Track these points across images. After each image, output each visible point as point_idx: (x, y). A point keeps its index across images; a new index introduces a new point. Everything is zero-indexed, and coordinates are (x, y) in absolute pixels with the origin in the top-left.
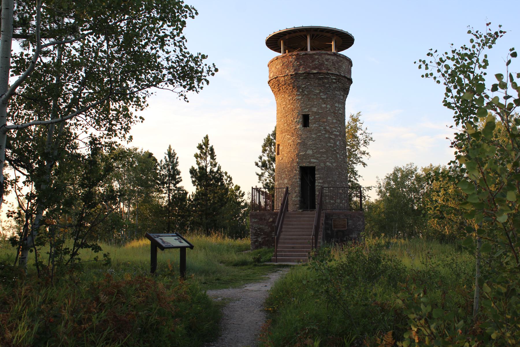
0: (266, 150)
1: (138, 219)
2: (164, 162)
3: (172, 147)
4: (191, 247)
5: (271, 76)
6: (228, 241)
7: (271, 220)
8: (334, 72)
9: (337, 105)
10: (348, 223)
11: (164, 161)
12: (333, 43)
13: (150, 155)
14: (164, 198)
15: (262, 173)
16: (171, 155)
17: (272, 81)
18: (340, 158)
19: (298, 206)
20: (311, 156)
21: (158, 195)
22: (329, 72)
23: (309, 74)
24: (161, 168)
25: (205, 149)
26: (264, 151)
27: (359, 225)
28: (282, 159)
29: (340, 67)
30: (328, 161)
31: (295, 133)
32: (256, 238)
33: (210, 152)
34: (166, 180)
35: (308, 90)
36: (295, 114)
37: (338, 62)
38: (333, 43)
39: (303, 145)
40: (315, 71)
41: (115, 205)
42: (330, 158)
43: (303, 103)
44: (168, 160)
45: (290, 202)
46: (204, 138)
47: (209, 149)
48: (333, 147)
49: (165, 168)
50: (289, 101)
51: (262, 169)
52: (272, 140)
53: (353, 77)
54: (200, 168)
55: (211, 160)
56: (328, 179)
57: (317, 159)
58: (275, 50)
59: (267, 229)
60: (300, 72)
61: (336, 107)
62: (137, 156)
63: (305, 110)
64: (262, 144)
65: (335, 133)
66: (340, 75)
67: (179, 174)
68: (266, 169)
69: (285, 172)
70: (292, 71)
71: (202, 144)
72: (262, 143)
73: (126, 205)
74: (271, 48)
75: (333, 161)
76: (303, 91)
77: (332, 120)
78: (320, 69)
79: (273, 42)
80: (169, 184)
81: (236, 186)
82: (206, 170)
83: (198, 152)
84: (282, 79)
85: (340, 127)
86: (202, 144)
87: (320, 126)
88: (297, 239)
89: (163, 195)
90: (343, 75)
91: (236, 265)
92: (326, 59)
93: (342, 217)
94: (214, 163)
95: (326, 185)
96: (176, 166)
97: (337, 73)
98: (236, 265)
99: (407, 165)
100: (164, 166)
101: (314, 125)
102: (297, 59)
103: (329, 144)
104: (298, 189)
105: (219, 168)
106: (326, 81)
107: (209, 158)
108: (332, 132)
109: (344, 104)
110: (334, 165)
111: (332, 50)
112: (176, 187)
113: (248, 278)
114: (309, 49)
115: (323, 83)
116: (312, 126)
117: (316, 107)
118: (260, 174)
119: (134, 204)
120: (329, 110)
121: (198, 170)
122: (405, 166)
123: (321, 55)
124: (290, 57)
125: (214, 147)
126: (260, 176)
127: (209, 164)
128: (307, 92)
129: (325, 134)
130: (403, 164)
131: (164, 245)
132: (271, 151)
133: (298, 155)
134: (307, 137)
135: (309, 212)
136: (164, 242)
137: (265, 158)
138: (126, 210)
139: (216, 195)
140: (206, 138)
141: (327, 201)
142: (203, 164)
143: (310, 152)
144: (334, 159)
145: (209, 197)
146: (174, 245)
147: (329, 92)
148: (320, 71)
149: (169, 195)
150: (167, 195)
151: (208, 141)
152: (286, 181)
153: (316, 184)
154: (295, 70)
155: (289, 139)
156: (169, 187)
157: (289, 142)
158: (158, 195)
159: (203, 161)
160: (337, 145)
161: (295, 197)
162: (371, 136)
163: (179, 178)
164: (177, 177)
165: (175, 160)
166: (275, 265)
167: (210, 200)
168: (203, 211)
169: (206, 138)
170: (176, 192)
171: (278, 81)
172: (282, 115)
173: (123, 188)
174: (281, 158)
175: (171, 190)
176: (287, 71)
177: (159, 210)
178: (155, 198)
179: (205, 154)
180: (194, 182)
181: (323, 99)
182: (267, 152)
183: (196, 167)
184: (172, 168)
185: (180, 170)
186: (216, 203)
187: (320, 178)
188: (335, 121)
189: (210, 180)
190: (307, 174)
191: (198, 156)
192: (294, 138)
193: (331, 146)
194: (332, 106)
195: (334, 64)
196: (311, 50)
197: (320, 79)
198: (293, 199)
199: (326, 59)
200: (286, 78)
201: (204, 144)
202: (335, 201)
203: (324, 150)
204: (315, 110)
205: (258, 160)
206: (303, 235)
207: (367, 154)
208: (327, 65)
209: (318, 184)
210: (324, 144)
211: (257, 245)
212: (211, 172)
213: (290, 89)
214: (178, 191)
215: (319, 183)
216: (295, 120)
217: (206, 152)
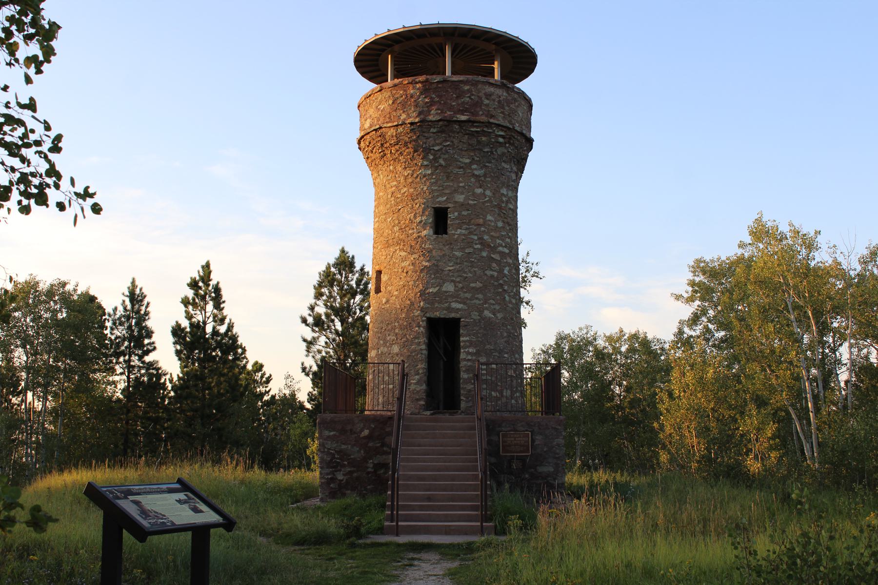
0: (322, 295)
1: (62, 424)
2: (120, 311)
3: (137, 283)
4: (229, 524)
5: (367, 125)
6: (258, 474)
7: (366, 432)
10: (533, 441)
11: (120, 309)
12: (496, 65)
13: (93, 299)
14: (117, 384)
15: (314, 338)
16: (135, 297)
17: (368, 137)
18: (510, 302)
19: (422, 403)
20: (452, 296)
21: (105, 377)
22: (492, 120)
23: (449, 122)
24: (114, 324)
25: (204, 289)
26: (319, 295)
27: (558, 445)
28: (387, 302)
29: (513, 112)
30: (487, 309)
31: (418, 246)
32: (332, 473)
33: (213, 295)
34: (123, 348)
35: (446, 156)
36: (418, 206)
37: (509, 103)
38: (496, 65)
39: (434, 272)
41: (18, 395)
42: (492, 301)
43: (436, 183)
44: (129, 307)
46: (203, 267)
47: (210, 288)
48: (497, 279)
49: (121, 324)
50: (406, 178)
51: (313, 331)
52: (335, 274)
53: (533, 135)
54: (192, 325)
55: (215, 311)
56: (488, 347)
57: (464, 303)
58: (371, 79)
59: (357, 453)
60: (431, 118)
61: (503, 194)
62: (66, 300)
64: (315, 283)
65: (501, 248)
66: (513, 130)
67: (150, 337)
68: (322, 329)
69: (394, 328)
70: (414, 114)
71: (198, 278)
72: (315, 279)
73: (39, 397)
74: (363, 74)
75: (497, 307)
76: (436, 159)
77: (496, 221)
78: (473, 114)
79: (371, 60)
80: (130, 356)
81: (256, 363)
82: (204, 328)
83: (190, 294)
84: (392, 131)
85: (509, 237)
86: (198, 278)
87: (471, 233)
88: (435, 478)
89: (116, 378)
90: (518, 129)
91: (301, 542)
92: (485, 94)
93: (522, 429)
94: (220, 317)
95: (483, 360)
96: (145, 320)
98: (301, 542)
99: (581, 329)
100: (119, 319)
101: (459, 231)
102: (425, 91)
103: (489, 273)
104: (422, 366)
105: (230, 327)
106: (484, 139)
107: (210, 307)
108: (495, 247)
109: (515, 189)
110: (500, 315)
111: (444, 73)
112: (143, 362)
114: (448, 72)
115: (479, 142)
116: (455, 232)
117: (462, 193)
118: (309, 339)
119: (56, 396)
120: (490, 201)
121: (188, 330)
122: (577, 330)
123: (475, 84)
124: (411, 87)
125: (221, 286)
126: (310, 344)
127: (211, 319)
128: (445, 160)
129: (481, 250)
130: (571, 328)
131: (145, 523)
132: (330, 296)
133: (422, 293)
134: (444, 255)
135: (447, 416)
136: (145, 513)
137: (321, 310)
138: (38, 405)
139: (222, 379)
140: (207, 267)
142: (199, 318)
143: (449, 287)
144: (500, 304)
145: (210, 383)
146: (179, 522)
148: (473, 118)
149: (128, 377)
150: (124, 377)
151: (210, 272)
152: (396, 349)
153: (462, 356)
154: (420, 114)
155: (404, 259)
156: (129, 360)
157: (403, 264)
158: (105, 377)
159: (198, 312)
160: (505, 275)
161: (417, 384)
162: (535, 268)
163: (149, 344)
164: (146, 341)
165: (143, 308)
166: (399, 545)
167: (210, 388)
168: (196, 410)
169: (207, 267)
170: (143, 371)
171: (382, 136)
172: (386, 210)
173: (34, 361)
174: (384, 300)
175: (134, 367)
176: (404, 116)
177: (106, 408)
178: (99, 383)
179: (203, 298)
180: (178, 353)
182: (324, 298)
183: (185, 324)
184: (137, 324)
185: (153, 329)
186: (222, 395)
187: (471, 344)
189: (212, 351)
190: (442, 334)
191: (189, 303)
192: (416, 256)
193: (492, 276)
194: (495, 192)
195: (501, 105)
197: (472, 134)
198: (412, 387)
199: (485, 94)
200: (400, 129)
201: (202, 279)
202: (501, 393)
203: (478, 285)
204: (460, 198)
205: (306, 313)
206: (447, 469)
207: (527, 303)
208: (487, 105)
209: (465, 355)
210: (479, 272)
211: (333, 488)
212: (215, 332)
213: (409, 154)
214: (148, 369)
215: (468, 353)
216: (418, 219)
217: (206, 294)
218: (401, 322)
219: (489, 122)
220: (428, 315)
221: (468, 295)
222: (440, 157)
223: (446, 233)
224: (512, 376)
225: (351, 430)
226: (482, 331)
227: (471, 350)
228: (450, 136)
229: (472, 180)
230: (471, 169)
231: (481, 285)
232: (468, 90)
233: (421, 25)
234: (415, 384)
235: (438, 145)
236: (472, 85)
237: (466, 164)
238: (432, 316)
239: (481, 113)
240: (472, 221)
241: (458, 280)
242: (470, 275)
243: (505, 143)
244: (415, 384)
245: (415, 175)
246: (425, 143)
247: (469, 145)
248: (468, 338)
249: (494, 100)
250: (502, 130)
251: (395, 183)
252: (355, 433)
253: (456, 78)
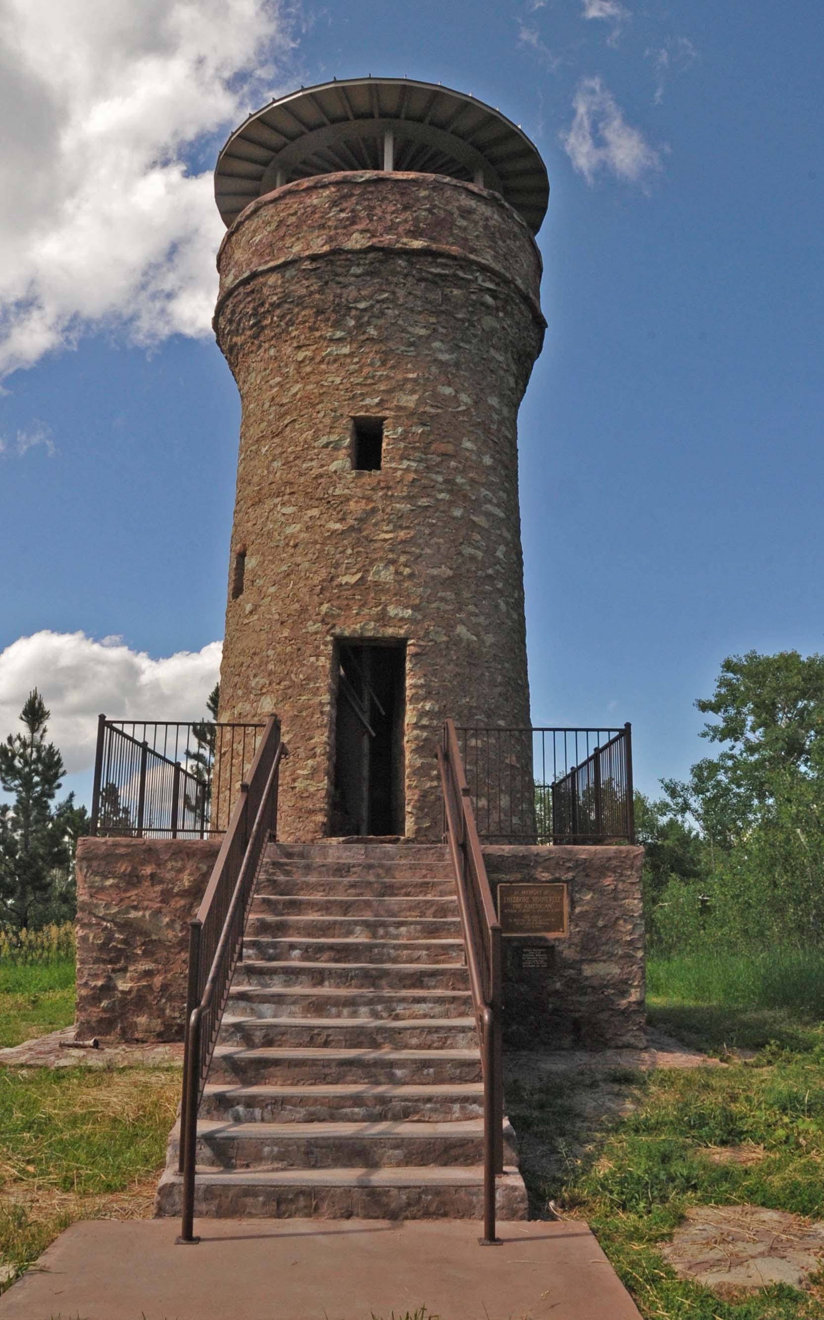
8: (487, 259)
23: (389, 253)
30: (462, 622)
35: (381, 322)
40: (417, 244)
45: (285, 802)
65: (489, 507)
76: (360, 326)
77: (480, 453)
101: (405, 464)
103: (468, 551)
104: (321, 738)
106: (456, 292)
113: (249, 288)
115: (446, 299)
117: (413, 392)
123: (437, 187)
129: (451, 503)
157: (289, 530)
161: (306, 779)
181: (442, 364)
193: (473, 558)
196: (397, 167)
197: (436, 281)
204: (409, 401)
208: (465, 229)
218: (279, 648)
220: (337, 631)
222: (369, 323)
223: (378, 468)
224: (513, 767)
225: (153, 876)
226: (450, 667)
228: (389, 283)
230: (430, 349)
231: (450, 573)
232: (425, 198)
234: (306, 778)
235: (364, 298)
236: (434, 189)
237: (420, 337)
238: (347, 633)
240: (433, 447)
243: (497, 309)
244: (306, 778)
245: (318, 359)
247: (427, 301)
249: (476, 223)
251: (278, 379)
252: (161, 882)
253: (400, 175)
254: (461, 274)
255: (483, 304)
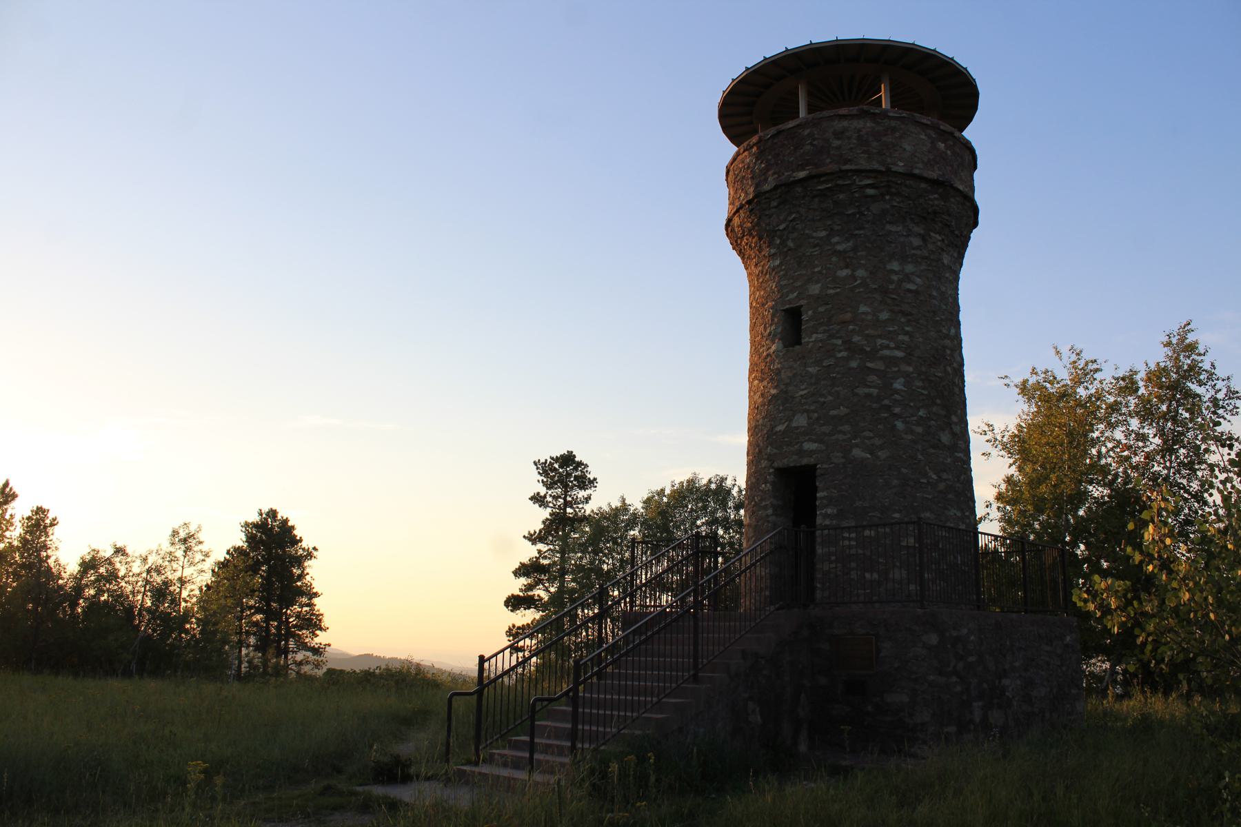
8: (864, 164)
9: (895, 266)
30: (857, 445)
35: (795, 235)
42: (867, 434)
53: (978, 197)
56: (858, 504)
57: (821, 441)
63: (792, 296)
65: (886, 352)
66: (888, 172)
75: (877, 442)
76: (783, 243)
85: (906, 333)
97: (876, 166)
101: (814, 336)
103: (862, 391)
106: (841, 196)
110: (882, 454)
116: (810, 339)
117: (817, 282)
141: (854, 575)
147: (861, 228)
153: (819, 521)
188: (884, 316)
193: (868, 396)
203: (843, 410)
204: (815, 289)
208: (839, 148)
215: (826, 516)
219: (841, 171)
220: (776, 465)
221: (826, 429)
222: (788, 239)
227: (829, 511)
229: (834, 259)
233: (747, 69)
239: (828, 160)
241: (812, 408)
242: (830, 398)
243: (882, 195)
246: (769, 224)
248: (825, 494)
249: (849, 138)
250: (869, 178)
254: (840, 182)
255: (867, 196)
